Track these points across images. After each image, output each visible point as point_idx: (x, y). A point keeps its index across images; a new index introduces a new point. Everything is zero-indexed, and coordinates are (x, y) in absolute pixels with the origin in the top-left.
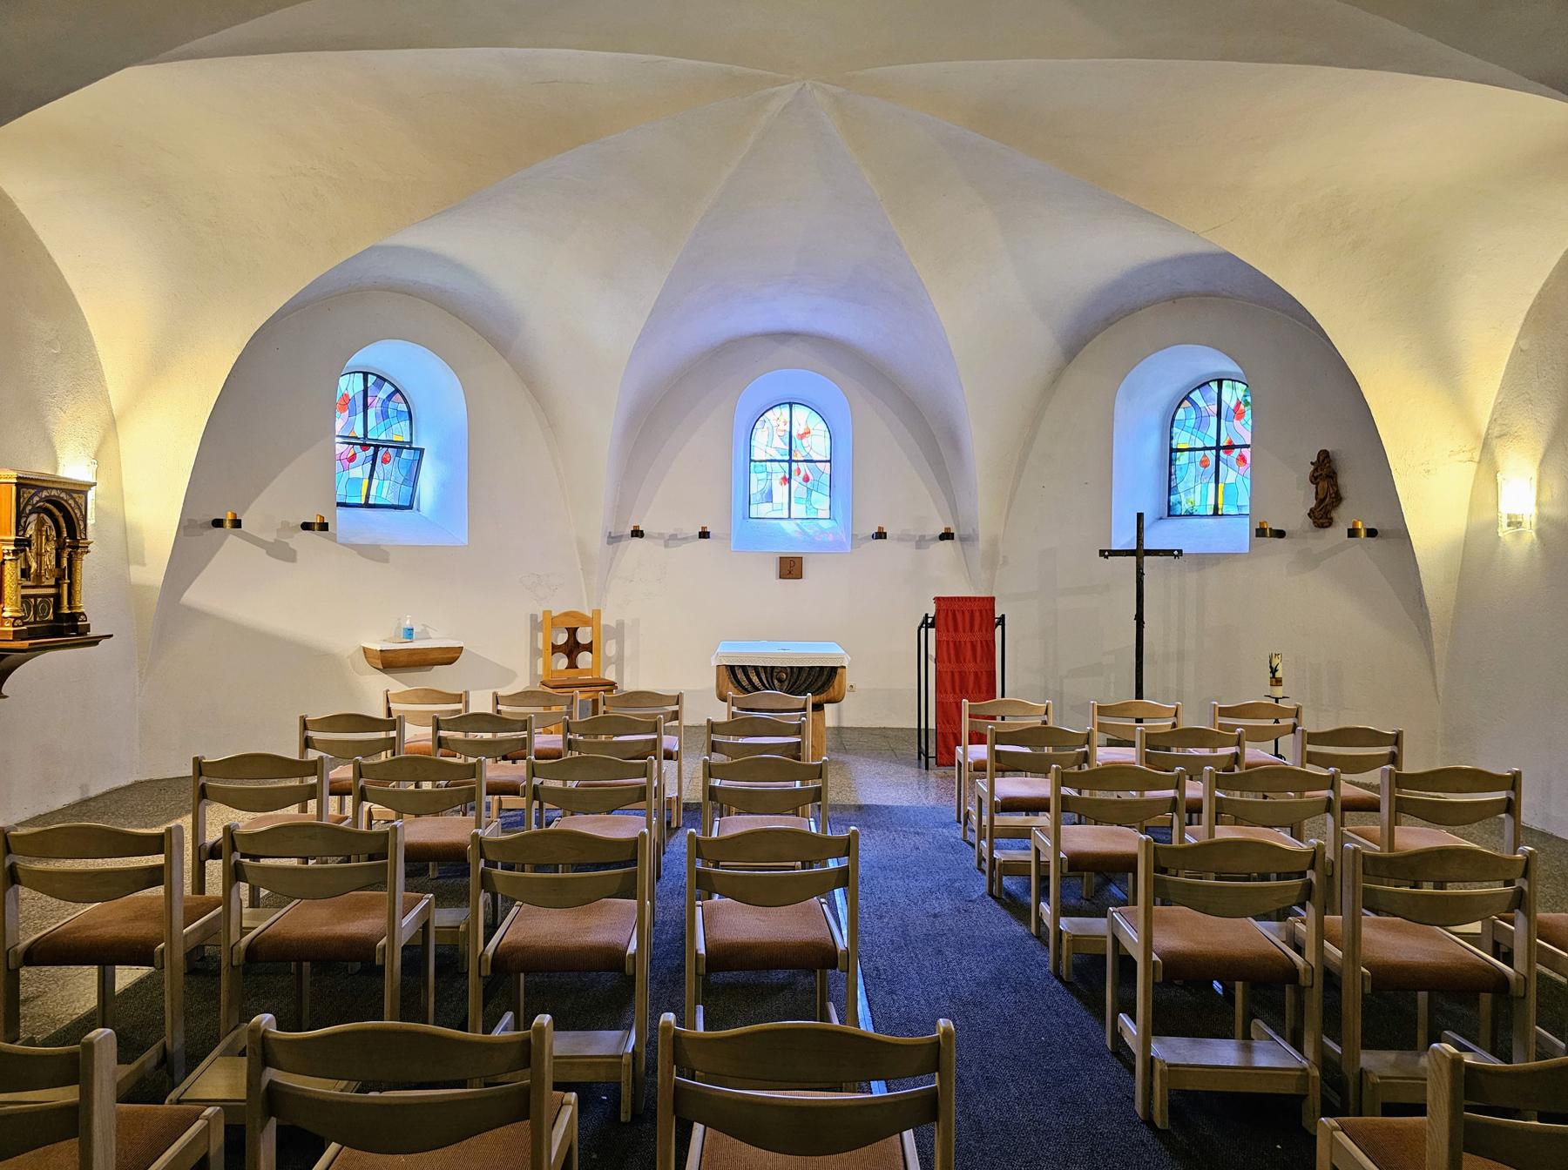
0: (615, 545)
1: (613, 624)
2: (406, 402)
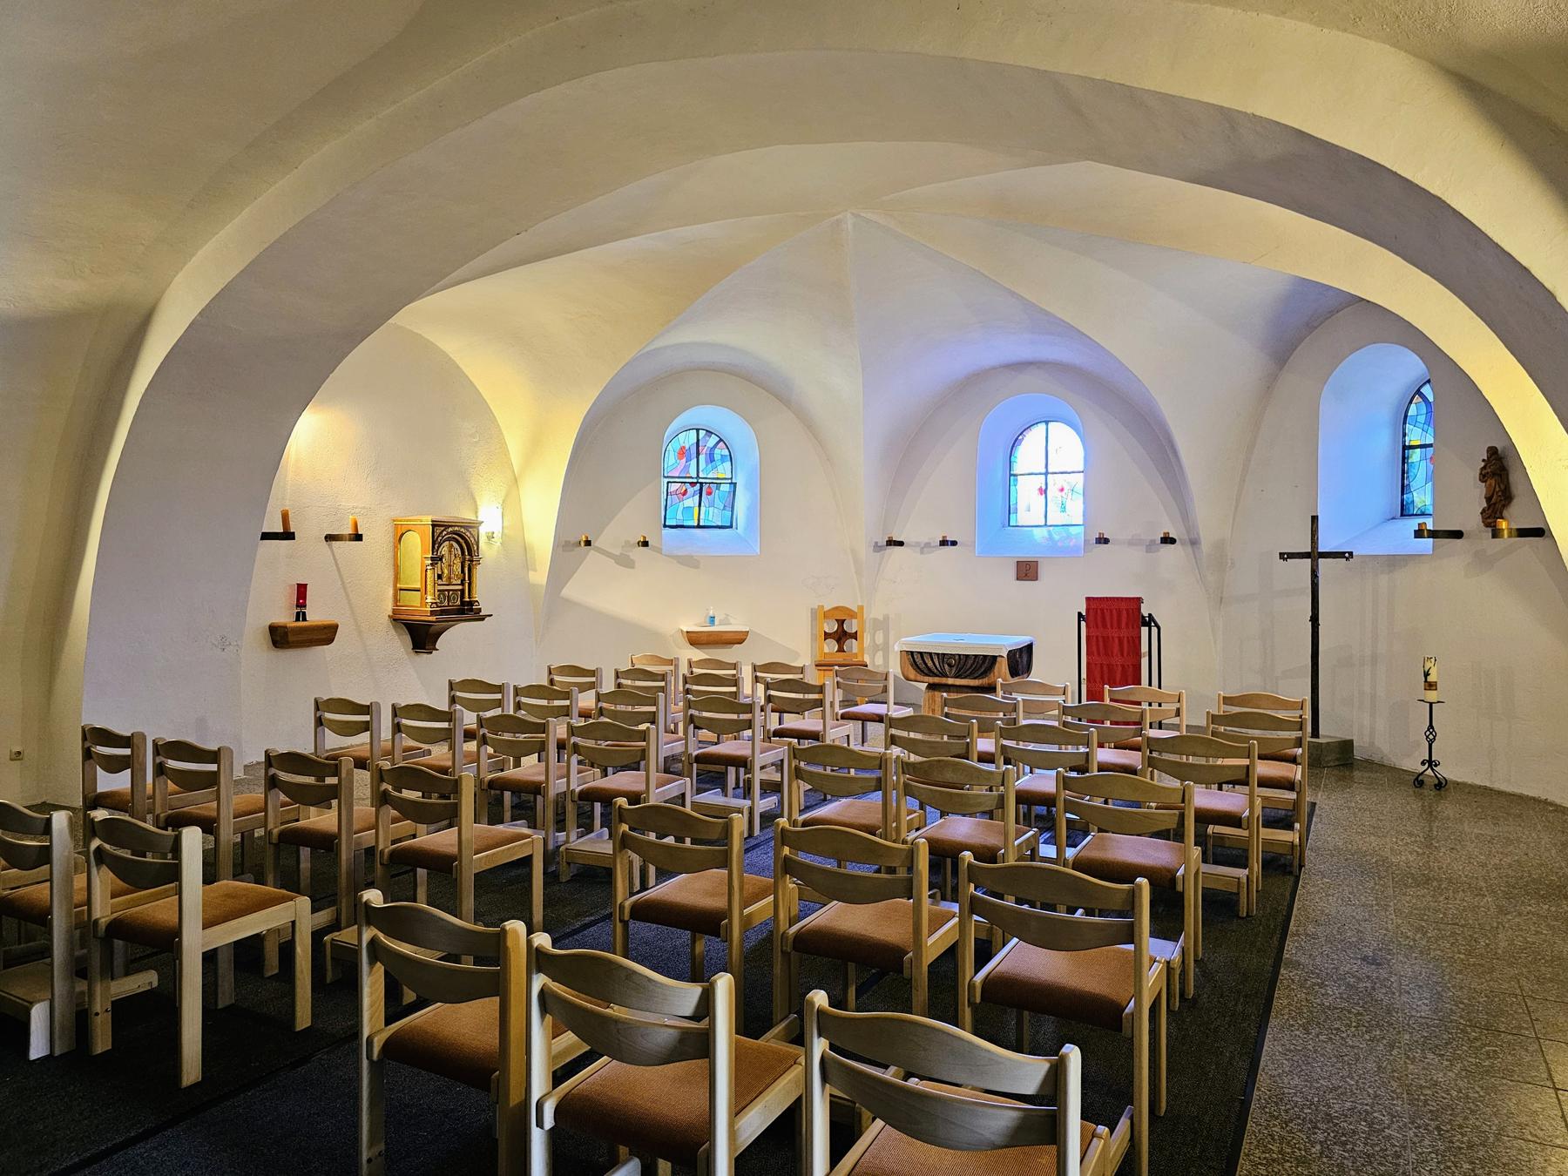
0: (882, 552)
1: (881, 618)
2: (728, 448)
